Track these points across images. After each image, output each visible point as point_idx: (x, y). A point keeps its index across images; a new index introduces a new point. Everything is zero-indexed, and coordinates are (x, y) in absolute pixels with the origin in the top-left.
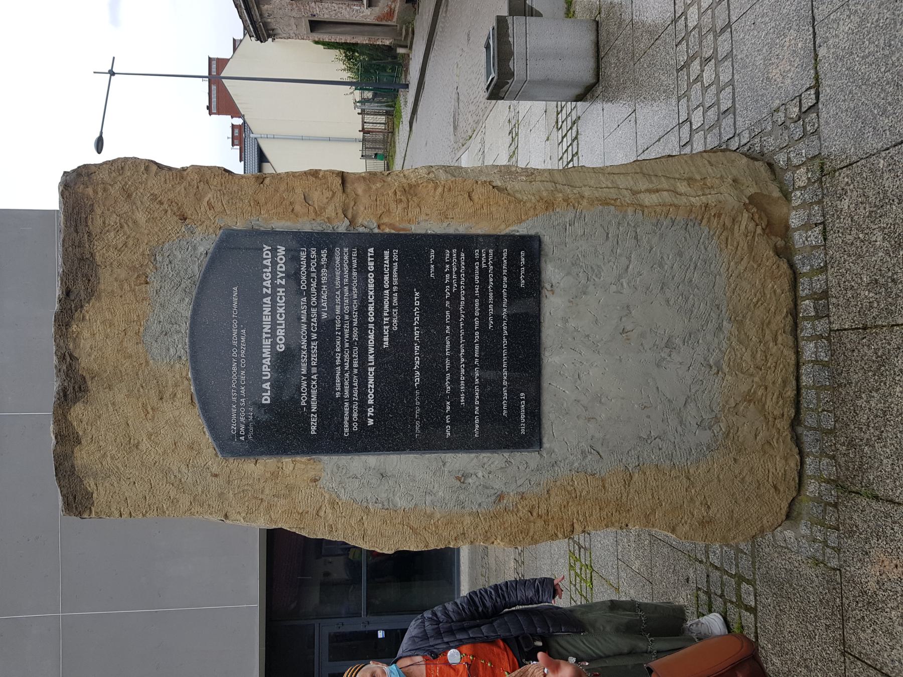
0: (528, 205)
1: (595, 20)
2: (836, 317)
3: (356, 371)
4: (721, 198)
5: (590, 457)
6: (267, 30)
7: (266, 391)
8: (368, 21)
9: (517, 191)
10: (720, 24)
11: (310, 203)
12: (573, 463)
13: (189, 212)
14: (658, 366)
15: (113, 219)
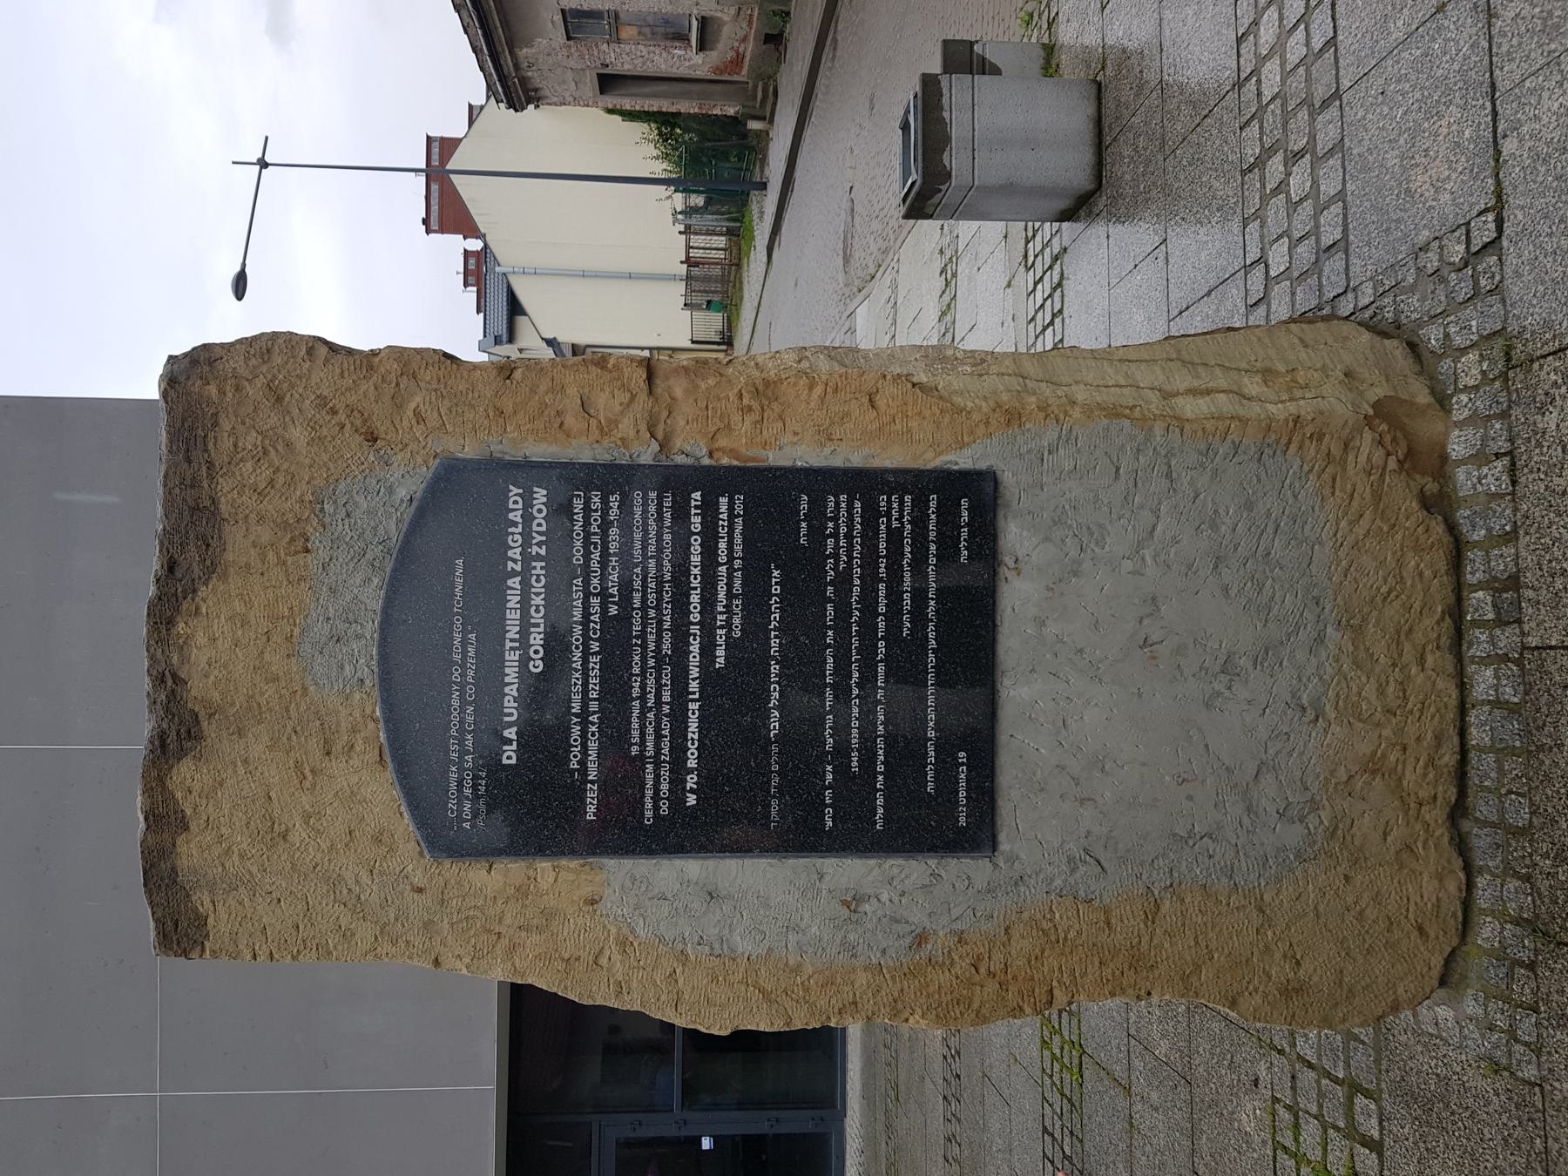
0: (976, 416)
1: (1094, 81)
2: (1533, 624)
3: (666, 709)
4: (1323, 405)
5: (1083, 869)
6: (526, 91)
7: (510, 742)
8: (699, 74)
9: (955, 392)
10: (1320, 93)
11: (592, 412)
12: (1052, 880)
13: (381, 428)
14: (1208, 706)
15: (251, 440)
